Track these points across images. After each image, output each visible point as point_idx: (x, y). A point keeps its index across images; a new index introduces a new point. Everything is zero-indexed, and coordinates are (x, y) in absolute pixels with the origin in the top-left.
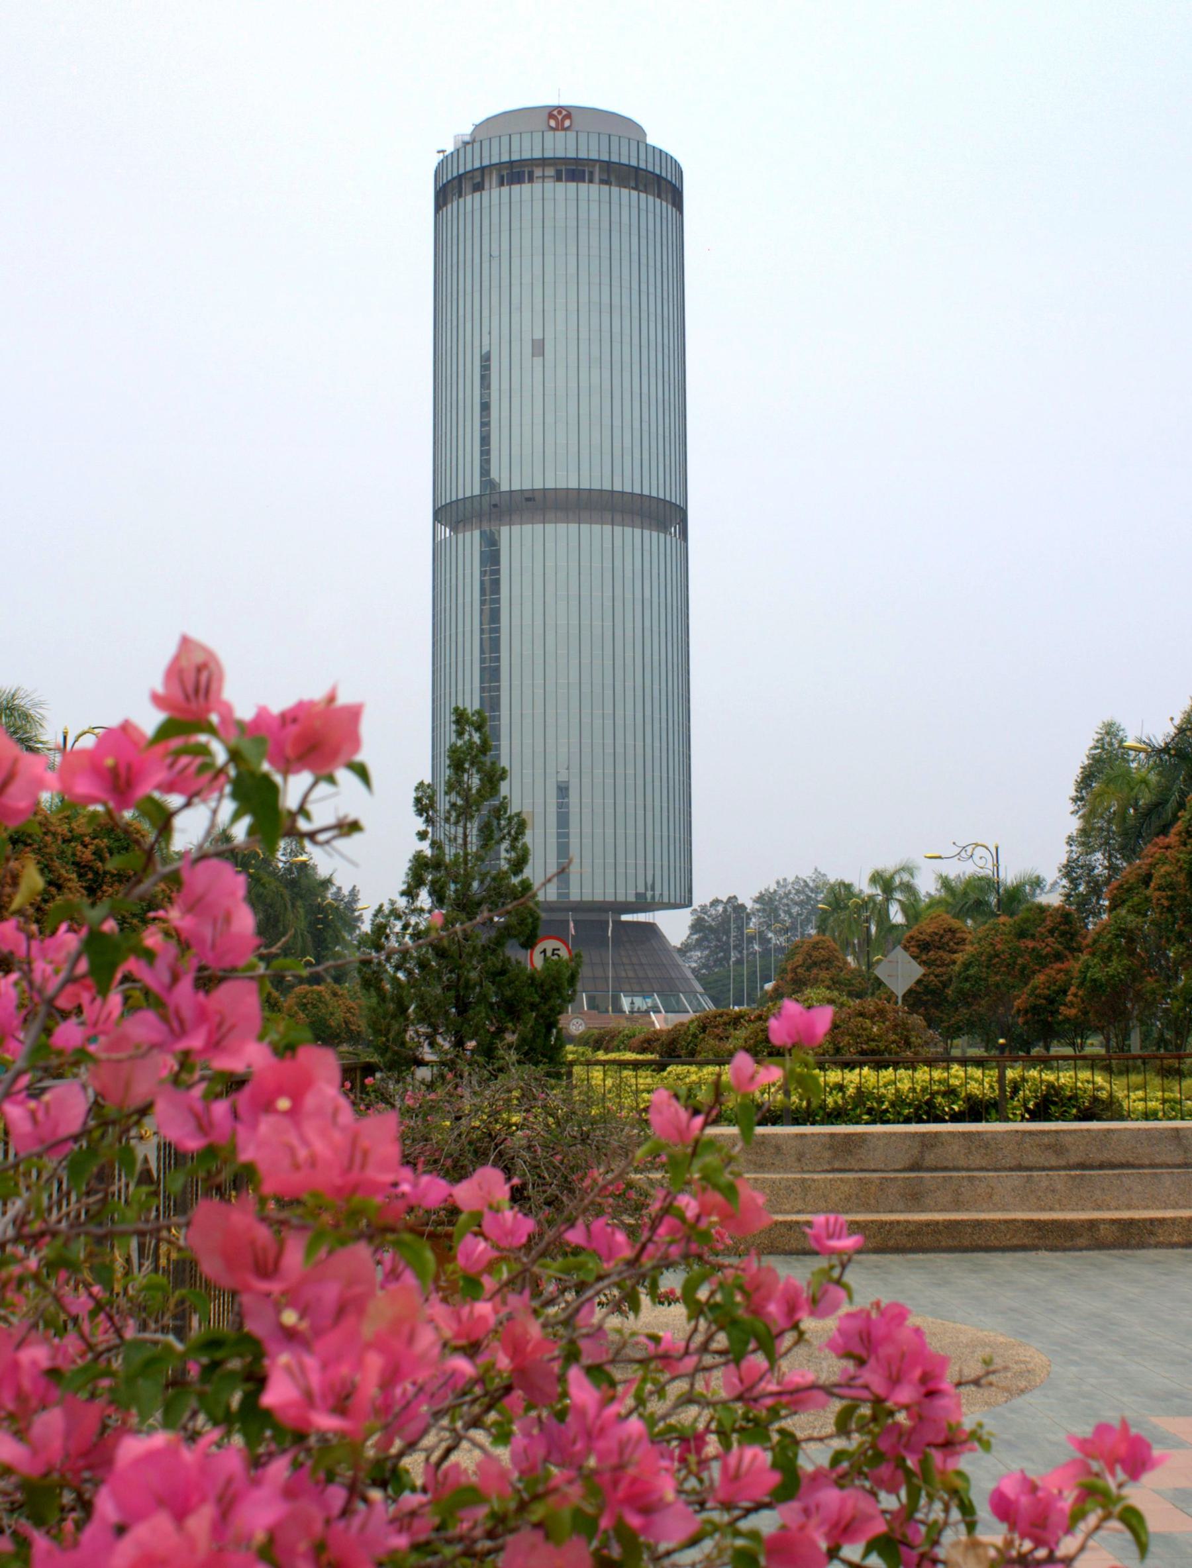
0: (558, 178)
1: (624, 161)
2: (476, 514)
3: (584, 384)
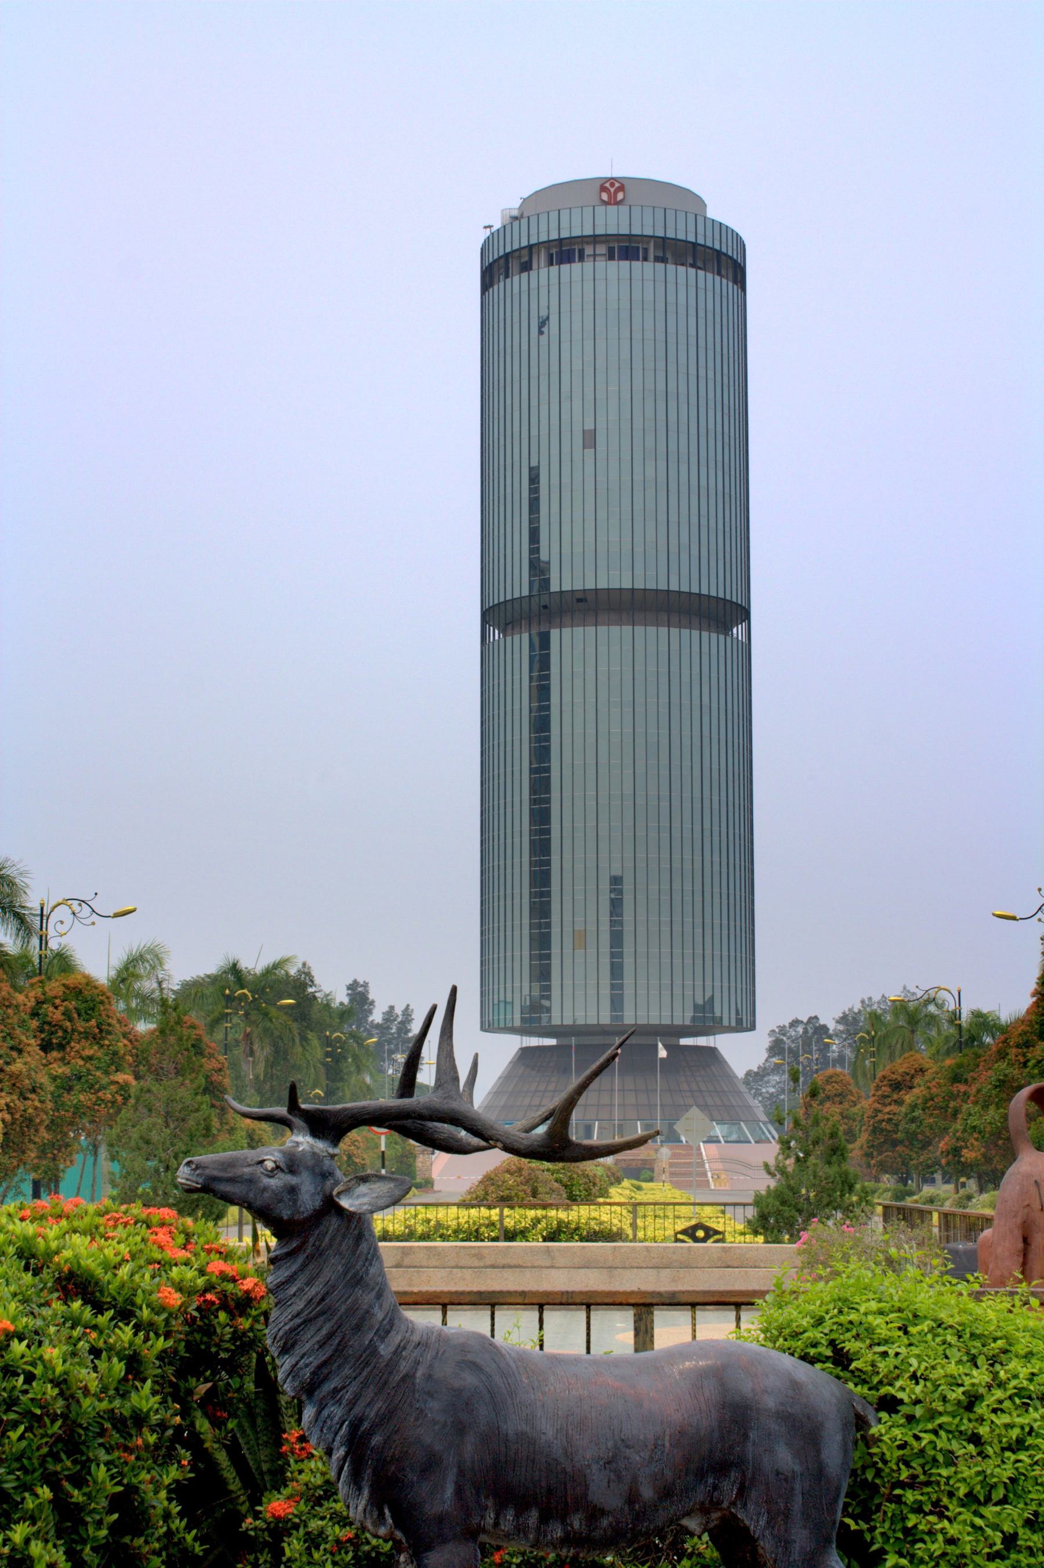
0: (611, 257)
1: (681, 236)
2: (526, 613)
3: (638, 477)
